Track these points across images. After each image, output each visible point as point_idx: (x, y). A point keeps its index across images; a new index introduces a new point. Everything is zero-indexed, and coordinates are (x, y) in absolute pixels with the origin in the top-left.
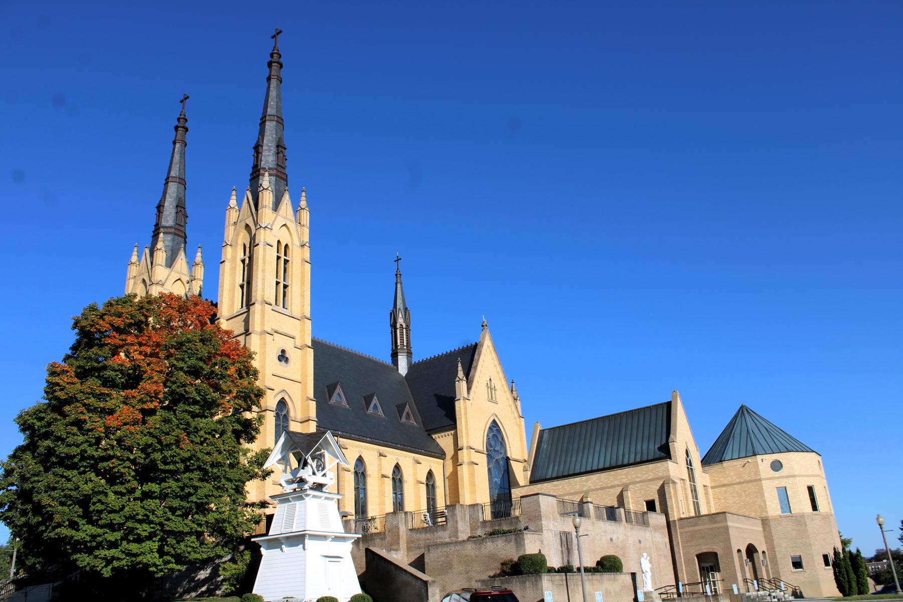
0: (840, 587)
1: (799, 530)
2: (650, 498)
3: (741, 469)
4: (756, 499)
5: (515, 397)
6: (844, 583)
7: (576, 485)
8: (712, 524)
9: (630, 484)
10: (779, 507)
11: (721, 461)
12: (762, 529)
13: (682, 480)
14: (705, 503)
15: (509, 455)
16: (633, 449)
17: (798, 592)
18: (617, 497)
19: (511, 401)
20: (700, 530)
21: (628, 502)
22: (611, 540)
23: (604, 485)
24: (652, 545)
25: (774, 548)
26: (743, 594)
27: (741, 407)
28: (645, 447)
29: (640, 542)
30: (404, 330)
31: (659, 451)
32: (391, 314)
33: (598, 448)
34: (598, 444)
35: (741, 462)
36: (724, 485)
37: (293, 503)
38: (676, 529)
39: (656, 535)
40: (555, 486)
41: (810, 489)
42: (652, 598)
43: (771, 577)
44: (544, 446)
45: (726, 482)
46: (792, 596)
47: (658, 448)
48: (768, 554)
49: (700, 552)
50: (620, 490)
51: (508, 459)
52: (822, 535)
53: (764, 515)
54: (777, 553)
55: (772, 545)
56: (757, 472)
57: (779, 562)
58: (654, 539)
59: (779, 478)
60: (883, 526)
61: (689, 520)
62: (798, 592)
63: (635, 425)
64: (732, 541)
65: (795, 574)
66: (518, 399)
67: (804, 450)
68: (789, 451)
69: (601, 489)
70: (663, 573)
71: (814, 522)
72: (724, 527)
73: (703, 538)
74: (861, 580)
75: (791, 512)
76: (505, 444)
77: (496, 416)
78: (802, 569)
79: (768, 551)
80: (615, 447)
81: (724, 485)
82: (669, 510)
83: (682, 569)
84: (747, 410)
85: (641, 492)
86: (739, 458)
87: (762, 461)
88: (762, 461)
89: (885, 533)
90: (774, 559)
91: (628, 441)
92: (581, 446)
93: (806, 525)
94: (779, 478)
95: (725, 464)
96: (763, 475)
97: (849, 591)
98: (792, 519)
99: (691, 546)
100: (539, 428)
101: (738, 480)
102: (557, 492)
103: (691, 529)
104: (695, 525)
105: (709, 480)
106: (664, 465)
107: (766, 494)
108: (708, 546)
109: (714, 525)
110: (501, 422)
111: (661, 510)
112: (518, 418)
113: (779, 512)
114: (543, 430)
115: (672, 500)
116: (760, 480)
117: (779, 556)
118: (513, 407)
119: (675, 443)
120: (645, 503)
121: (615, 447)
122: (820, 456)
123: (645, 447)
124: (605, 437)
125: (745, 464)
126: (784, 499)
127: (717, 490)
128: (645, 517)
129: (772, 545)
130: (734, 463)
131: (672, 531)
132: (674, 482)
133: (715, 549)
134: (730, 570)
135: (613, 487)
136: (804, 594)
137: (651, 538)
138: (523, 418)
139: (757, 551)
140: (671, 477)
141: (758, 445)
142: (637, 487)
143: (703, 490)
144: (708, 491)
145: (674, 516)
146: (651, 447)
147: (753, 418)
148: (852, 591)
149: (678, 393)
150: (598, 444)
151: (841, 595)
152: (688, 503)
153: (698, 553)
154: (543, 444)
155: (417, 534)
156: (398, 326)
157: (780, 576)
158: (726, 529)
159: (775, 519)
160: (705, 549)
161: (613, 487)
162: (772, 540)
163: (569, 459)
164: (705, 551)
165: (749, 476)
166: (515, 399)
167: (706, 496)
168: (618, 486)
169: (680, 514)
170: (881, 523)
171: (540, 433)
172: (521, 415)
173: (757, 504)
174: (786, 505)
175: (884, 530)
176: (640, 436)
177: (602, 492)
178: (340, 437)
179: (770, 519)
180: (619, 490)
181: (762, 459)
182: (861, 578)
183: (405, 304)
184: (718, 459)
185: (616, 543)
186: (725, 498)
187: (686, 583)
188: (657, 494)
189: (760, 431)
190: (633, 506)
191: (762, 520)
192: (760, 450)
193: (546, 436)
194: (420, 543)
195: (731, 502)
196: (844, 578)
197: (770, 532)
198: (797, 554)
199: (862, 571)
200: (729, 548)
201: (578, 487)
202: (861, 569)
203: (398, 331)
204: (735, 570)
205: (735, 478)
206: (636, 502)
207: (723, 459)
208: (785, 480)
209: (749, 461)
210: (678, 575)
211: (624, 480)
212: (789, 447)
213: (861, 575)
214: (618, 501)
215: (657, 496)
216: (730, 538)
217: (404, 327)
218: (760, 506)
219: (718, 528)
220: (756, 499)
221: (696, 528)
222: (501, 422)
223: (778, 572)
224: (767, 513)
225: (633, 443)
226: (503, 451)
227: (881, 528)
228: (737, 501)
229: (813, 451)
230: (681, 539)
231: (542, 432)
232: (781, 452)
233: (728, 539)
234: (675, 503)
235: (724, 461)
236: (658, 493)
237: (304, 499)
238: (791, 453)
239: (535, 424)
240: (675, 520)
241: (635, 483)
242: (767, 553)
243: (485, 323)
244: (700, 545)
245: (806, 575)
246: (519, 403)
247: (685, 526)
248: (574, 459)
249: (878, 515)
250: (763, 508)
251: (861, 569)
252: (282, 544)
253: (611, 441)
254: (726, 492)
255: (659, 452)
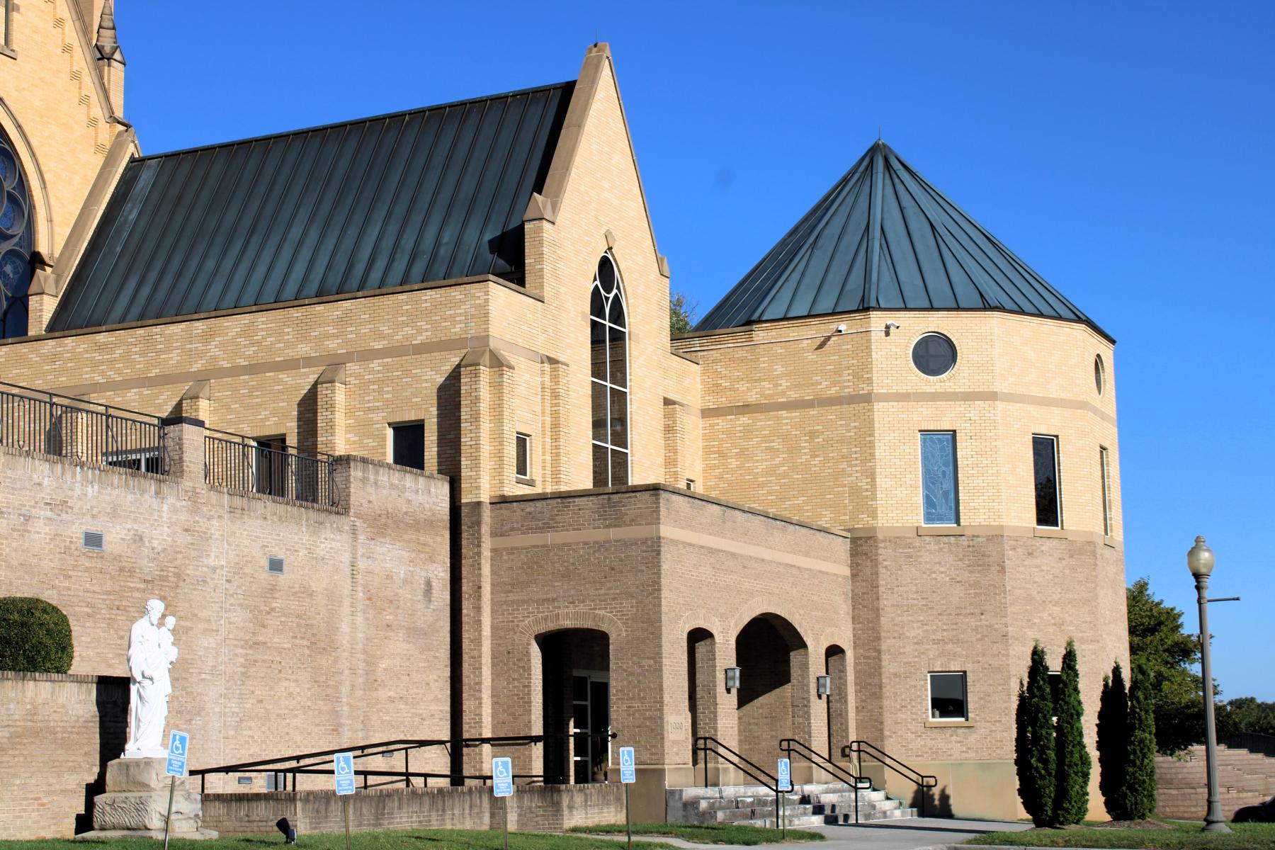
0: (1030, 794)
1: (976, 585)
2: (410, 416)
3: (811, 356)
4: (844, 465)
5: (107, 50)
6: (1042, 777)
7: (169, 350)
8: (607, 527)
9: (349, 357)
10: (920, 500)
11: (749, 323)
12: (846, 571)
13: (552, 361)
14: (661, 460)
16: (408, 242)
17: (937, 797)
18: (299, 405)
19: (81, 60)
20: (561, 547)
21: (331, 426)
22: (93, 540)
23: (263, 357)
24: (347, 584)
25: (879, 639)
26: (672, 792)
27: (869, 150)
28: (447, 237)
29: (276, 565)
31: (492, 252)
33: (296, 231)
34: (304, 214)
35: (815, 330)
36: (746, 408)
38: (479, 538)
39: (380, 550)
40: (100, 348)
41: (1045, 450)
42: (145, 786)
43: (853, 737)
44: (131, 213)
45: (752, 397)
46: (912, 806)
47: (491, 242)
48: (856, 658)
49: (552, 626)
50: (312, 378)
52: (1056, 610)
53: (864, 521)
54: (885, 658)
55: (873, 629)
56: (863, 371)
57: (887, 691)
58: (361, 564)
59: (935, 397)
60: (1207, 582)
61: (530, 507)
62: (937, 797)
63: (439, 157)
64: (665, 594)
65: (936, 734)
66: (117, 56)
67: (1045, 309)
68: (987, 307)
69: (253, 369)
70: (383, 694)
71: (1037, 561)
72: (645, 541)
73: (566, 576)
74: (1131, 770)
75: (958, 522)
76: (32, 207)
78: (963, 719)
79: (856, 646)
80: (352, 232)
81: (746, 408)
82: (464, 462)
83: (480, 683)
84: (886, 160)
85: (380, 391)
86: (808, 316)
87: (887, 334)
88: (887, 334)
89: (1208, 607)
90: (871, 675)
91: (400, 211)
92: (247, 221)
93: (1002, 569)
94: (935, 397)
95: (761, 334)
96: (881, 383)
97: (1054, 810)
98: (957, 545)
99: (524, 602)
100: (130, 150)
101: (794, 395)
102: (102, 373)
103: (534, 539)
104: (547, 527)
105: (699, 386)
106: (473, 297)
107: (880, 451)
108: (582, 608)
109: (614, 533)
110: (19, 127)
111: (440, 464)
113: (915, 515)
114: (142, 160)
115: (478, 428)
116: (867, 398)
117: (889, 667)
118: (89, 81)
119: (546, 225)
120: (390, 433)
121: (352, 232)
122: (1113, 342)
123: (447, 237)
124: (331, 195)
125: (829, 338)
126: (944, 473)
127: (721, 423)
128: (338, 478)
129: (873, 629)
130: (791, 332)
131: (464, 542)
132: (498, 363)
133: (602, 619)
134: (642, 699)
135: (291, 365)
136: (956, 806)
137: (346, 558)
139: (803, 645)
140: (492, 344)
141: (887, 277)
142: (372, 372)
143: (661, 415)
144: (674, 422)
145: (478, 488)
146: (471, 236)
147: (899, 187)
148: (1067, 810)
149: (608, 52)
150: (304, 214)
151: (1108, 818)
152: (557, 447)
153: (544, 628)
157: (882, 738)
158: (654, 547)
159: (897, 540)
160: (568, 618)
161: (291, 365)
162: (877, 612)
163: (193, 264)
164: (568, 624)
165: (834, 384)
166: (102, 57)
167: (667, 439)
168: (308, 362)
169: (501, 482)
170: (1203, 570)
171: (127, 169)
172: (119, 113)
173: (847, 480)
174: (946, 494)
175: (1207, 594)
176: (445, 195)
177: (253, 381)
179: (880, 536)
180: (305, 380)
181: (888, 327)
182: (1135, 765)
184: (742, 317)
185: (117, 558)
186: (743, 454)
187: (487, 734)
188: (435, 401)
189: (909, 234)
190: (347, 440)
191: (854, 540)
192: (888, 294)
193: (146, 178)
195: (761, 467)
196: (1046, 762)
197: (873, 585)
198: (955, 666)
199: (1141, 741)
200: (651, 623)
201: (174, 357)
202: (1138, 733)
204: (661, 702)
205: (784, 384)
206: (362, 428)
207: (755, 317)
208: (960, 407)
209: (843, 327)
210: (461, 704)
211: (332, 345)
212: (993, 294)
213: (1134, 752)
214: (299, 419)
215: (434, 411)
216: (659, 583)
218: (855, 491)
219: (626, 544)
220: (844, 465)
221: (551, 538)
222: (19, 127)
223: (878, 725)
224: (875, 518)
225: (417, 218)
226: (18, 230)
227: (1199, 588)
228: (781, 464)
229: (1079, 319)
230: (493, 572)
231: (136, 164)
232: (958, 309)
233: (655, 588)
234: (493, 439)
235: (760, 321)
236: (439, 397)
238: (996, 314)
240: (479, 504)
241: (367, 356)
242: (849, 654)
244: (554, 600)
245: (973, 738)
246: (116, 74)
247: (512, 529)
248: (210, 264)
249: (1198, 540)
250: (864, 498)
251: (1138, 733)
253: (346, 206)
254: (748, 431)
255: (490, 257)
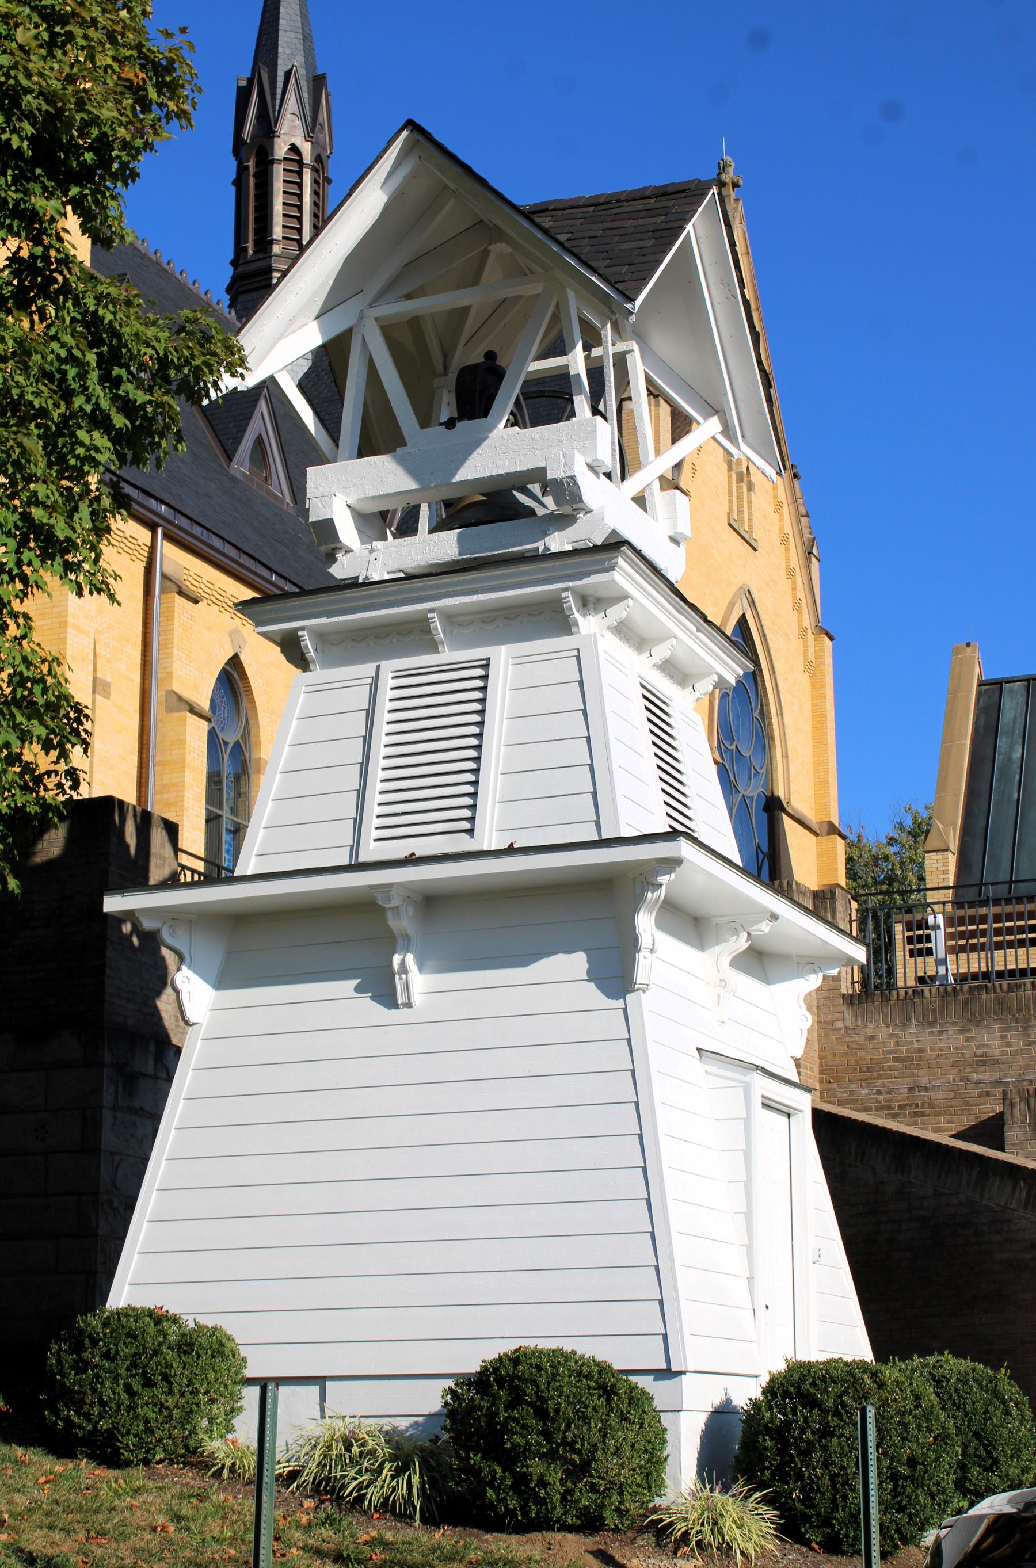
15: (780, 793)
30: (307, 177)
32: (243, 97)
37: (447, 655)
51: (773, 806)
76: (772, 738)
77: (752, 603)
112: (811, 637)
114: (999, 683)
138: (831, 638)
154: (1002, 743)
155: (904, 1026)
156: (281, 149)
171: (979, 694)
178: (167, 536)
183: (313, 58)
194: (925, 1081)
203: (279, 175)
217: (307, 159)
237: (565, 626)
239: (956, 651)
243: (731, 170)
252: (391, 942)
